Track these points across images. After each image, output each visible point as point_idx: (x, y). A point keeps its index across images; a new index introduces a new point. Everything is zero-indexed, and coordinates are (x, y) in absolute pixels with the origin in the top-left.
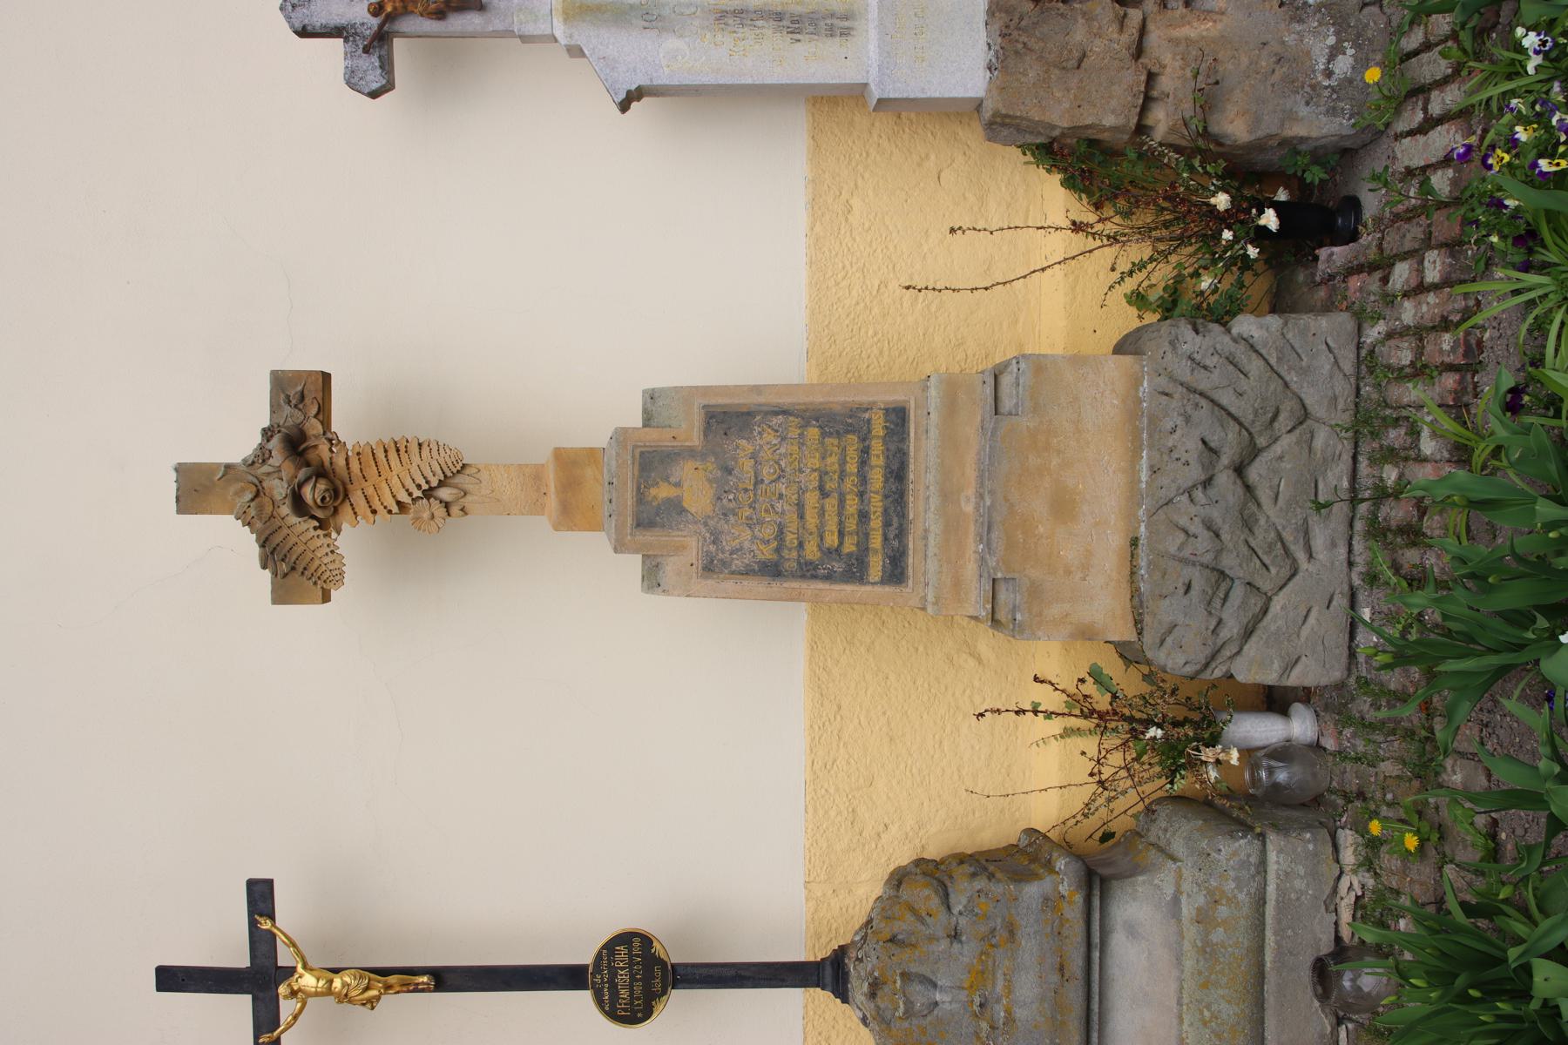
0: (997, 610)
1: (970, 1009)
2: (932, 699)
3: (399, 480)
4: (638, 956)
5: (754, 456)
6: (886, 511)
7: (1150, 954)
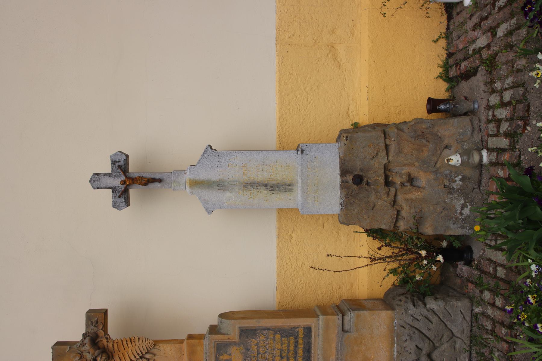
5: (257, 345)
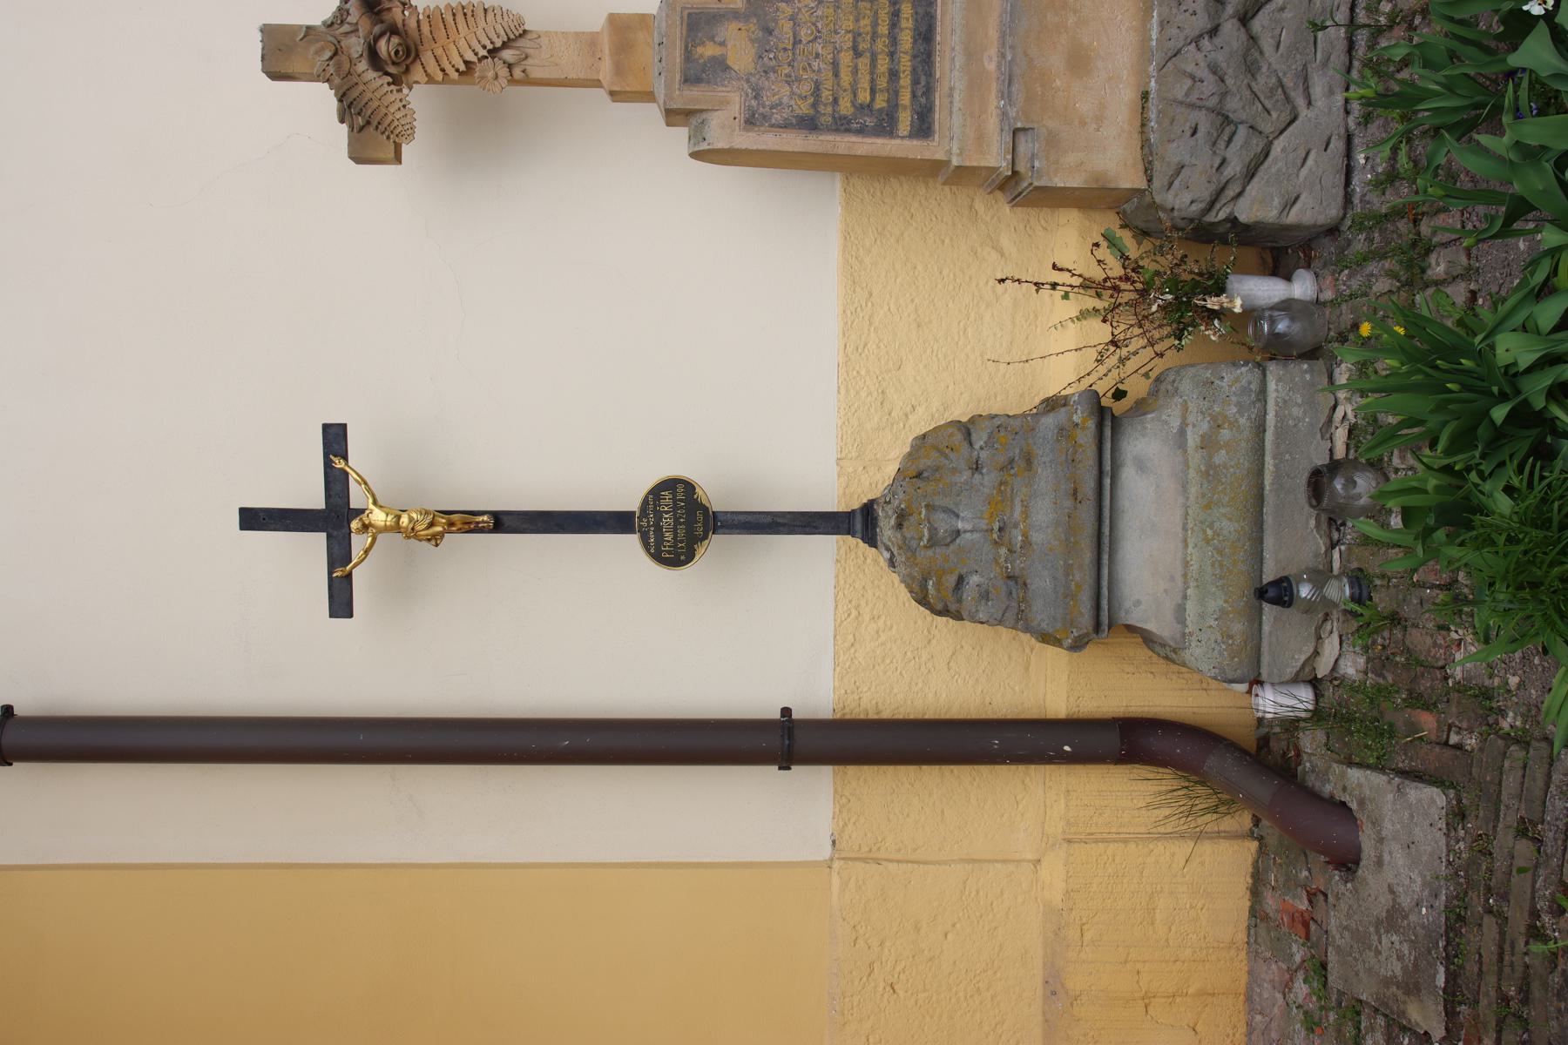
0: (1017, 161)
1: (990, 538)
2: (957, 289)
3: (464, 45)
4: (681, 500)
5: (793, 18)
6: (914, 70)
7: (1158, 487)
